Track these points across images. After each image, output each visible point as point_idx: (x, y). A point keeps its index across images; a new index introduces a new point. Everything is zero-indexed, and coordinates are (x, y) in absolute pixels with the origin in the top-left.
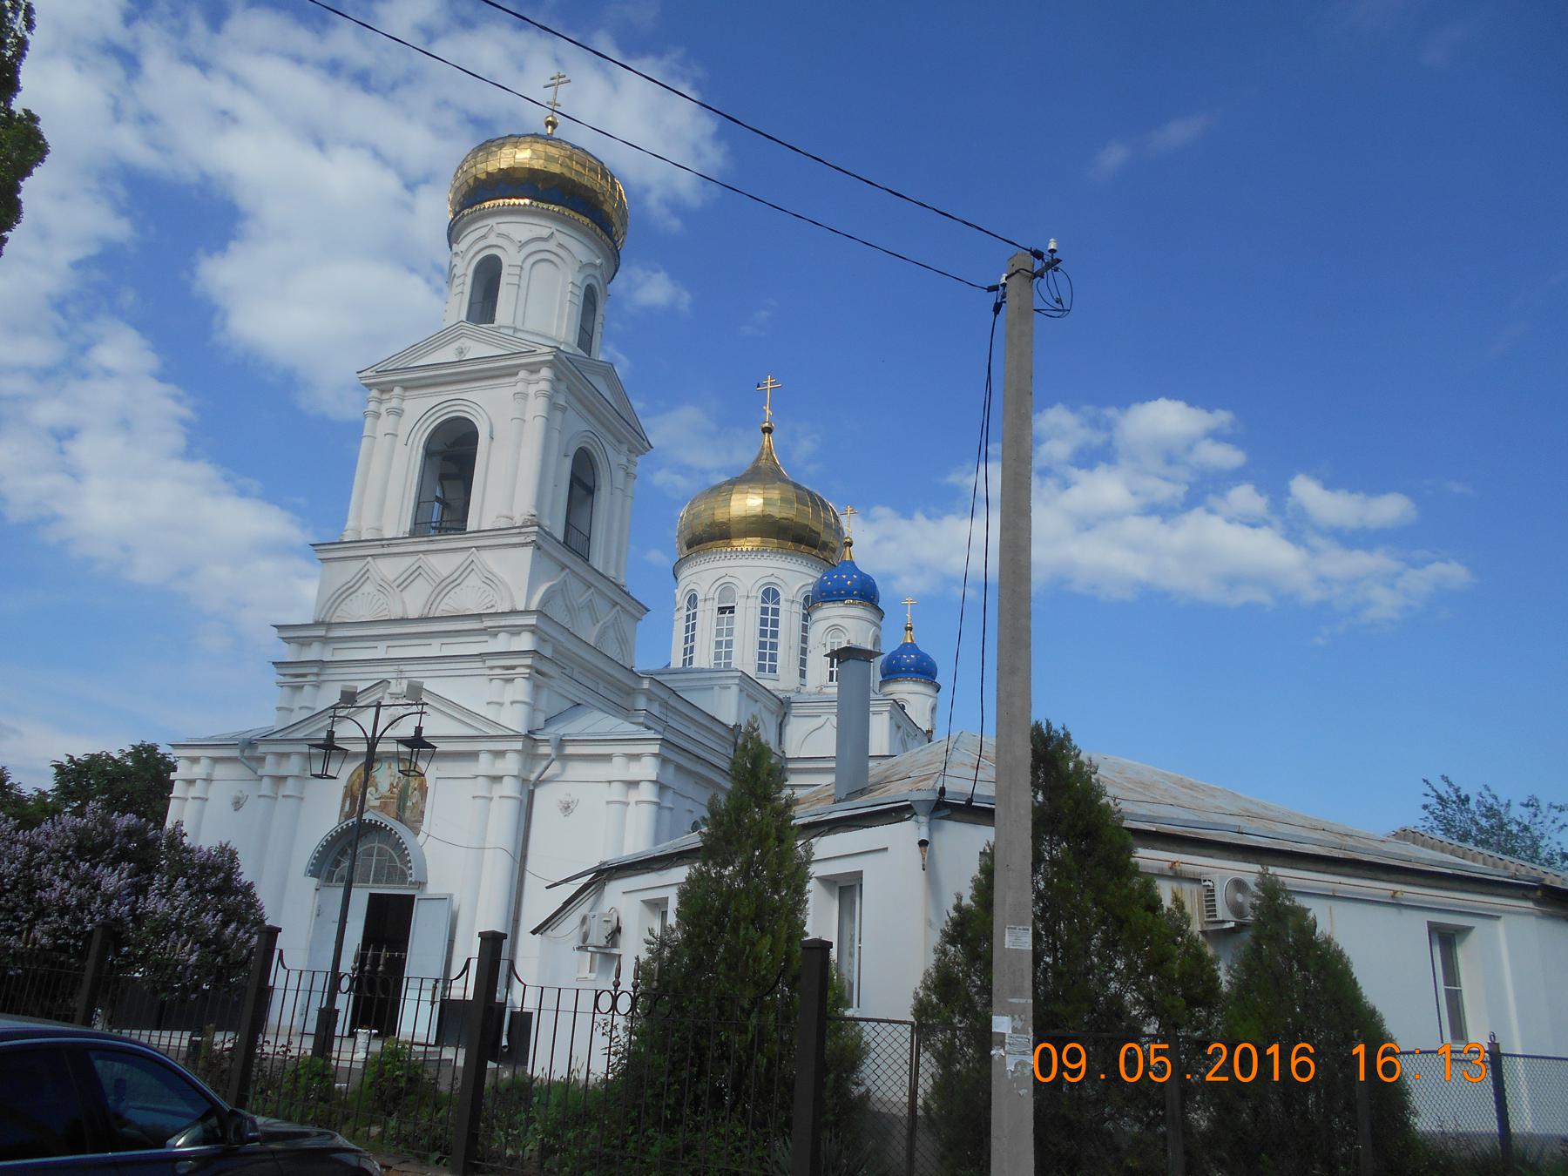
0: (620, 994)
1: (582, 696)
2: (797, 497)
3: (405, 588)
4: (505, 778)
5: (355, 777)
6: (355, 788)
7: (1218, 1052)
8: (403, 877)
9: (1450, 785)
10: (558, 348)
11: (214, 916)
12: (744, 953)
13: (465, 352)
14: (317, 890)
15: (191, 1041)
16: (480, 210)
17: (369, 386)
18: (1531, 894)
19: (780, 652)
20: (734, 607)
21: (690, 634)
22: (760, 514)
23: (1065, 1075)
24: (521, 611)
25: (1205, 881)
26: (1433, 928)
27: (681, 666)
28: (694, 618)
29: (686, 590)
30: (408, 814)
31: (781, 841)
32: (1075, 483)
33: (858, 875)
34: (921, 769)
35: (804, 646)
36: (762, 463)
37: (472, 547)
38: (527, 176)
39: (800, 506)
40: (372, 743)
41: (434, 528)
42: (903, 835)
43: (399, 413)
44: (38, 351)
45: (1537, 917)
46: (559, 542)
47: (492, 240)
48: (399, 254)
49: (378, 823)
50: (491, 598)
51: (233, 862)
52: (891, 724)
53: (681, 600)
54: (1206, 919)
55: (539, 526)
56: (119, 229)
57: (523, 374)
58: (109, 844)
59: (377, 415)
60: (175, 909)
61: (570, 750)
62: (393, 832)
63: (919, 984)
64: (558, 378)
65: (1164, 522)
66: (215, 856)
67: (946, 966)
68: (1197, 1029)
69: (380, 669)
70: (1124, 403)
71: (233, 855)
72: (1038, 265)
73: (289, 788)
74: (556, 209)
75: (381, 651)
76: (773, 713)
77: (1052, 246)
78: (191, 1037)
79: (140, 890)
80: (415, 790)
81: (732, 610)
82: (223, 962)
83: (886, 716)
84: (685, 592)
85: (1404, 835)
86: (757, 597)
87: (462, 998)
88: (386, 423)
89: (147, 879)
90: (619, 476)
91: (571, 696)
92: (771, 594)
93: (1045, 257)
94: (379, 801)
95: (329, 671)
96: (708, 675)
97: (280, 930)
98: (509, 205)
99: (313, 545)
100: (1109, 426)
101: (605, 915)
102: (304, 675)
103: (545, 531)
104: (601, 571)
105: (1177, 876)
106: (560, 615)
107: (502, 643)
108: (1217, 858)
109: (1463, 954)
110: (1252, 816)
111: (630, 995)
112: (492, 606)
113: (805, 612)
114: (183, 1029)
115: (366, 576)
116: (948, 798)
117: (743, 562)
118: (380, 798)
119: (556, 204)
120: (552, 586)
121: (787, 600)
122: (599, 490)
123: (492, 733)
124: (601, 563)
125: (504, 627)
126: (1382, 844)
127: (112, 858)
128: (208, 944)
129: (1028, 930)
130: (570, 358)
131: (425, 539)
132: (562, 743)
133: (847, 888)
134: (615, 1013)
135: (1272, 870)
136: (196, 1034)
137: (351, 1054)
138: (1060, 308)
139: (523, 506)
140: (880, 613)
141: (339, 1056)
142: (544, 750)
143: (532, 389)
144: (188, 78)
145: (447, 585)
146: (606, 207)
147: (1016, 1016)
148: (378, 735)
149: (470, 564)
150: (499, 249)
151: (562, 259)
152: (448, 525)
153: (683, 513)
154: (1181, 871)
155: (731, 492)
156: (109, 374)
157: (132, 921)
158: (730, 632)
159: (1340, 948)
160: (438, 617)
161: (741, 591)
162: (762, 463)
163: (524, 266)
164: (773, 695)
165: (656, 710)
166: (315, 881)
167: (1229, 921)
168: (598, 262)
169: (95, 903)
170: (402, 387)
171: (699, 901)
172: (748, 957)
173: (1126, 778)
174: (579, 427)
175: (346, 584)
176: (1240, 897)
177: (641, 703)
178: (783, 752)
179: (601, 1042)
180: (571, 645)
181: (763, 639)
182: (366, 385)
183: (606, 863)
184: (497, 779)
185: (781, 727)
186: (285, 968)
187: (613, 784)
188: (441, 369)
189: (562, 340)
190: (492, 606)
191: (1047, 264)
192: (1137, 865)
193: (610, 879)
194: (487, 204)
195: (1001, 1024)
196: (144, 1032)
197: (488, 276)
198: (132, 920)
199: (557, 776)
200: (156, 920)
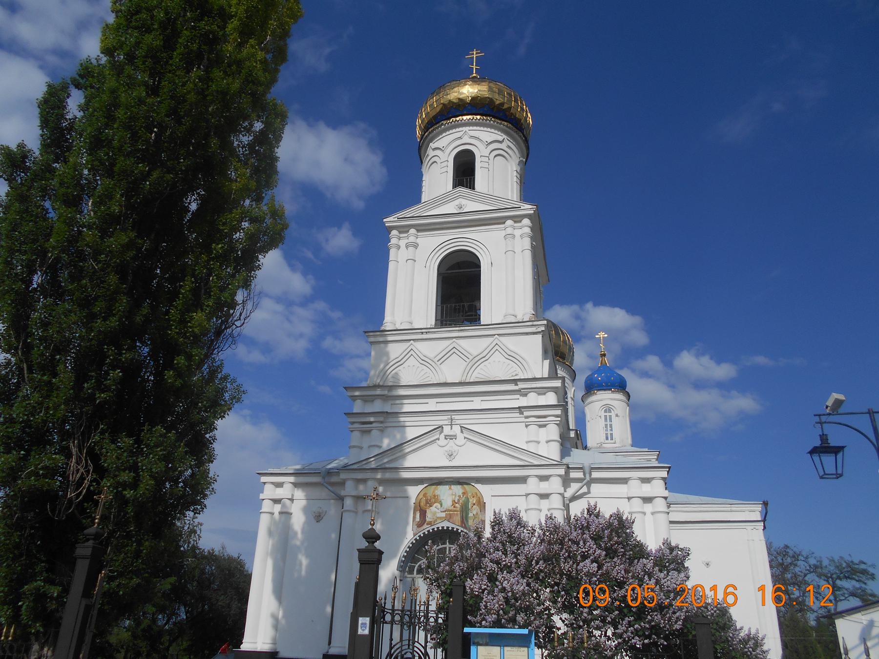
5: (421, 496)
6: (422, 504)
14: (401, 580)
24: (540, 378)
30: (470, 522)
37: (495, 335)
47: (466, 139)
70: (597, 304)
80: (474, 504)
87: (478, 647)
95: (391, 420)
107: (533, 399)
112: (516, 375)
123: (536, 463)
143: (518, 233)
151: (510, 156)
184: (544, 496)
190: (516, 375)
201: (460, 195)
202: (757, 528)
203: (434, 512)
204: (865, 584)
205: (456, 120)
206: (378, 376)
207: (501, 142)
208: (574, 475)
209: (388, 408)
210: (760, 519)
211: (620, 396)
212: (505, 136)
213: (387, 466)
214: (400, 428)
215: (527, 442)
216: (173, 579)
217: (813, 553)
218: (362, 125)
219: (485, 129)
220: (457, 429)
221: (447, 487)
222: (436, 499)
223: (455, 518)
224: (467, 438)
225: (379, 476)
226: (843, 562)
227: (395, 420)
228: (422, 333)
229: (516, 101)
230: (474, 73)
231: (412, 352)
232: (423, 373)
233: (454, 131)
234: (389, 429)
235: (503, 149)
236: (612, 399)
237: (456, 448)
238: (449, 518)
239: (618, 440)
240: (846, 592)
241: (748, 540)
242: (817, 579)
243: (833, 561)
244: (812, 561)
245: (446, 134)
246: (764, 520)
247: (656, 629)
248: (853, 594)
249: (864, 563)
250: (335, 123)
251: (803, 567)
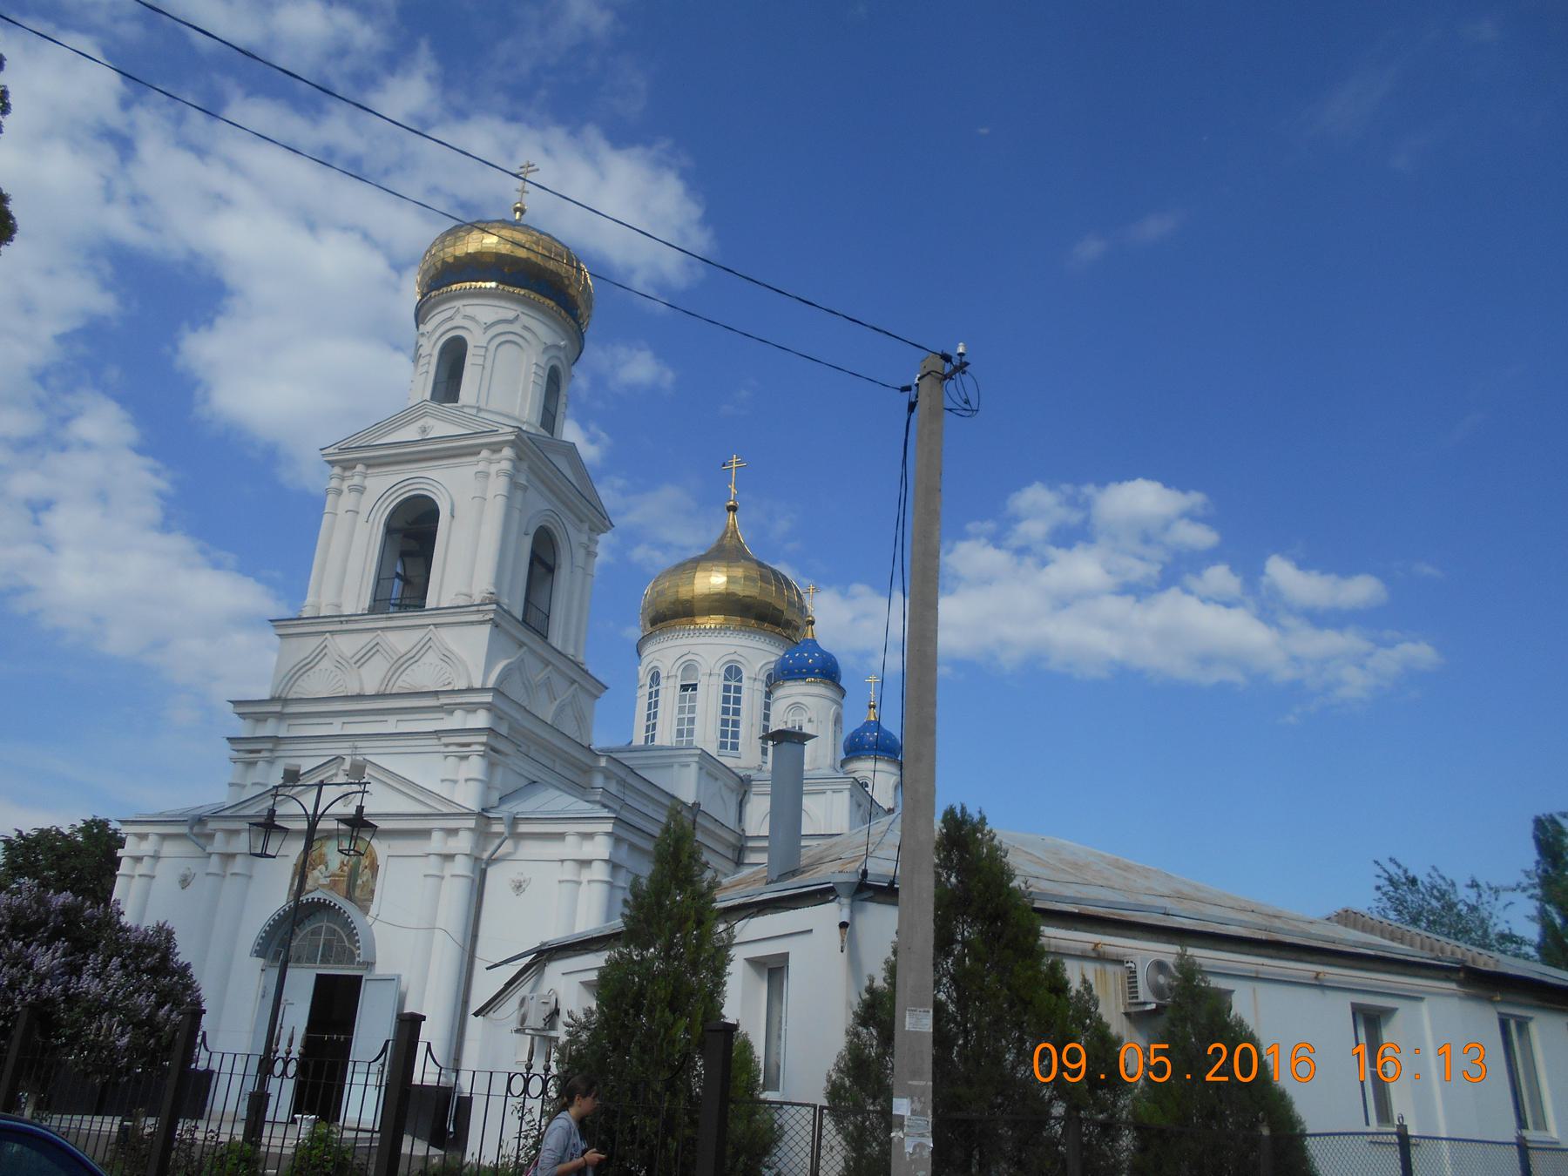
0: (532, 1077)
1: (539, 774)
2: (760, 575)
3: (362, 664)
4: (457, 856)
7: (1218, 1051)
8: (350, 957)
9: (1399, 866)
10: (520, 428)
11: (148, 997)
12: (659, 1036)
14: (262, 970)
15: (121, 1125)
16: (447, 292)
17: (332, 463)
18: (1454, 976)
19: (742, 730)
20: (696, 685)
21: (652, 711)
22: (724, 592)
23: (1065, 1074)
25: (1127, 962)
26: (1358, 1011)
27: (643, 743)
28: (657, 696)
29: (650, 667)
30: (358, 893)
31: (700, 923)
32: (1053, 561)
33: (785, 957)
34: (853, 851)
35: (766, 723)
36: (727, 541)
37: (430, 625)
38: (493, 260)
39: (764, 585)
40: (313, 820)
41: (394, 605)
42: (828, 915)
43: (360, 490)
44: (15, 422)
45: (1460, 998)
46: (517, 620)
47: (458, 321)
48: (379, 331)
49: (327, 902)
50: (447, 675)
51: (169, 942)
52: (851, 802)
53: (645, 679)
54: (1129, 1001)
55: (498, 604)
56: (103, 303)
57: (485, 453)
58: (45, 923)
59: (339, 492)
60: (108, 989)
61: (523, 828)
62: (342, 911)
63: (833, 1067)
64: (519, 458)
65: (1138, 600)
66: (152, 936)
67: (857, 1047)
68: (1101, 1112)
70: (1102, 484)
71: (170, 934)
72: (948, 368)
73: (239, 865)
74: (522, 292)
75: (336, 728)
76: (733, 791)
77: (961, 350)
78: (122, 1122)
79: (75, 970)
80: (366, 868)
81: (694, 687)
82: (156, 1044)
83: (846, 794)
84: (648, 670)
85: (1347, 918)
86: (719, 675)
88: (348, 500)
89: (83, 959)
90: (580, 554)
91: (525, 774)
92: (733, 672)
93: (953, 360)
94: (328, 879)
95: (283, 747)
96: (669, 753)
97: (424, 1018)
98: (475, 288)
99: (271, 621)
100: (1086, 505)
101: (545, 996)
102: (259, 751)
103: (503, 609)
104: (559, 649)
105: (1099, 957)
106: (516, 692)
107: (457, 720)
108: (1140, 940)
109: (1387, 1034)
110: (1180, 897)
111: (541, 1077)
112: (449, 683)
113: (767, 689)
114: (114, 1115)
115: (324, 652)
116: (870, 880)
117: (707, 640)
118: (330, 877)
119: (522, 287)
120: (508, 664)
121: (749, 678)
122: (559, 567)
123: (445, 810)
124: (560, 642)
126: (1310, 926)
127: (47, 937)
128: (133, 1021)
129: (928, 1012)
130: (532, 438)
131: (384, 616)
132: (515, 821)
133: (773, 970)
134: (527, 1096)
135: (1190, 951)
136: (127, 1118)
137: (110, 1126)
138: (968, 408)
139: (483, 584)
140: (842, 692)
141: (270, 1142)
142: (497, 828)
143: (494, 468)
144: (182, 165)
145: (402, 663)
146: (572, 291)
147: (916, 1098)
148: (320, 812)
149: (374, 646)
150: (464, 330)
151: (526, 340)
152: (407, 602)
153: (647, 590)
154: (1104, 953)
155: (695, 569)
156: (87, 446)
157: (64, 1001)
158: (692, 709)
159: (1250, 1030)
160: (395, 694)
161: (703, 669)
162: (727, 541)
163: (490, 347)
164: (733, 773)
165: (613, 788)
166: (261, 961)
167: (1150, 1003)
168: (562, 343)
169: (27, 983)
170: (365, 464)
171: (617, 984)
172: (663, 1040)
173: (1060, 859)
174: (540, 506)
175: (304, 660)
176: (1162, 979)
177: (599, 781)
178: (743, 830)
179: (513, 1124)
180: (528, 723)
181: (725, 717)
182: (329, 462)
183: (547, 943)
184: (449, 857)
185: (741, 805)
186: (207, 1050)
187: (566, 863)
188: (405, 447)
189: (525, 420)
190: (449, 683)
191: (956, 367)
192: (1042, 946)
193: (550, 959)
194: (454, 287)
195: (901, 1107)
196: (86, 1118)
197: (453, 357)
198: (64, 1000)
199: (509, 854)
200: (88, 1001)
201: (426, 412)
228: (341, 622)
236: (805, 695)
250: (621, 136)
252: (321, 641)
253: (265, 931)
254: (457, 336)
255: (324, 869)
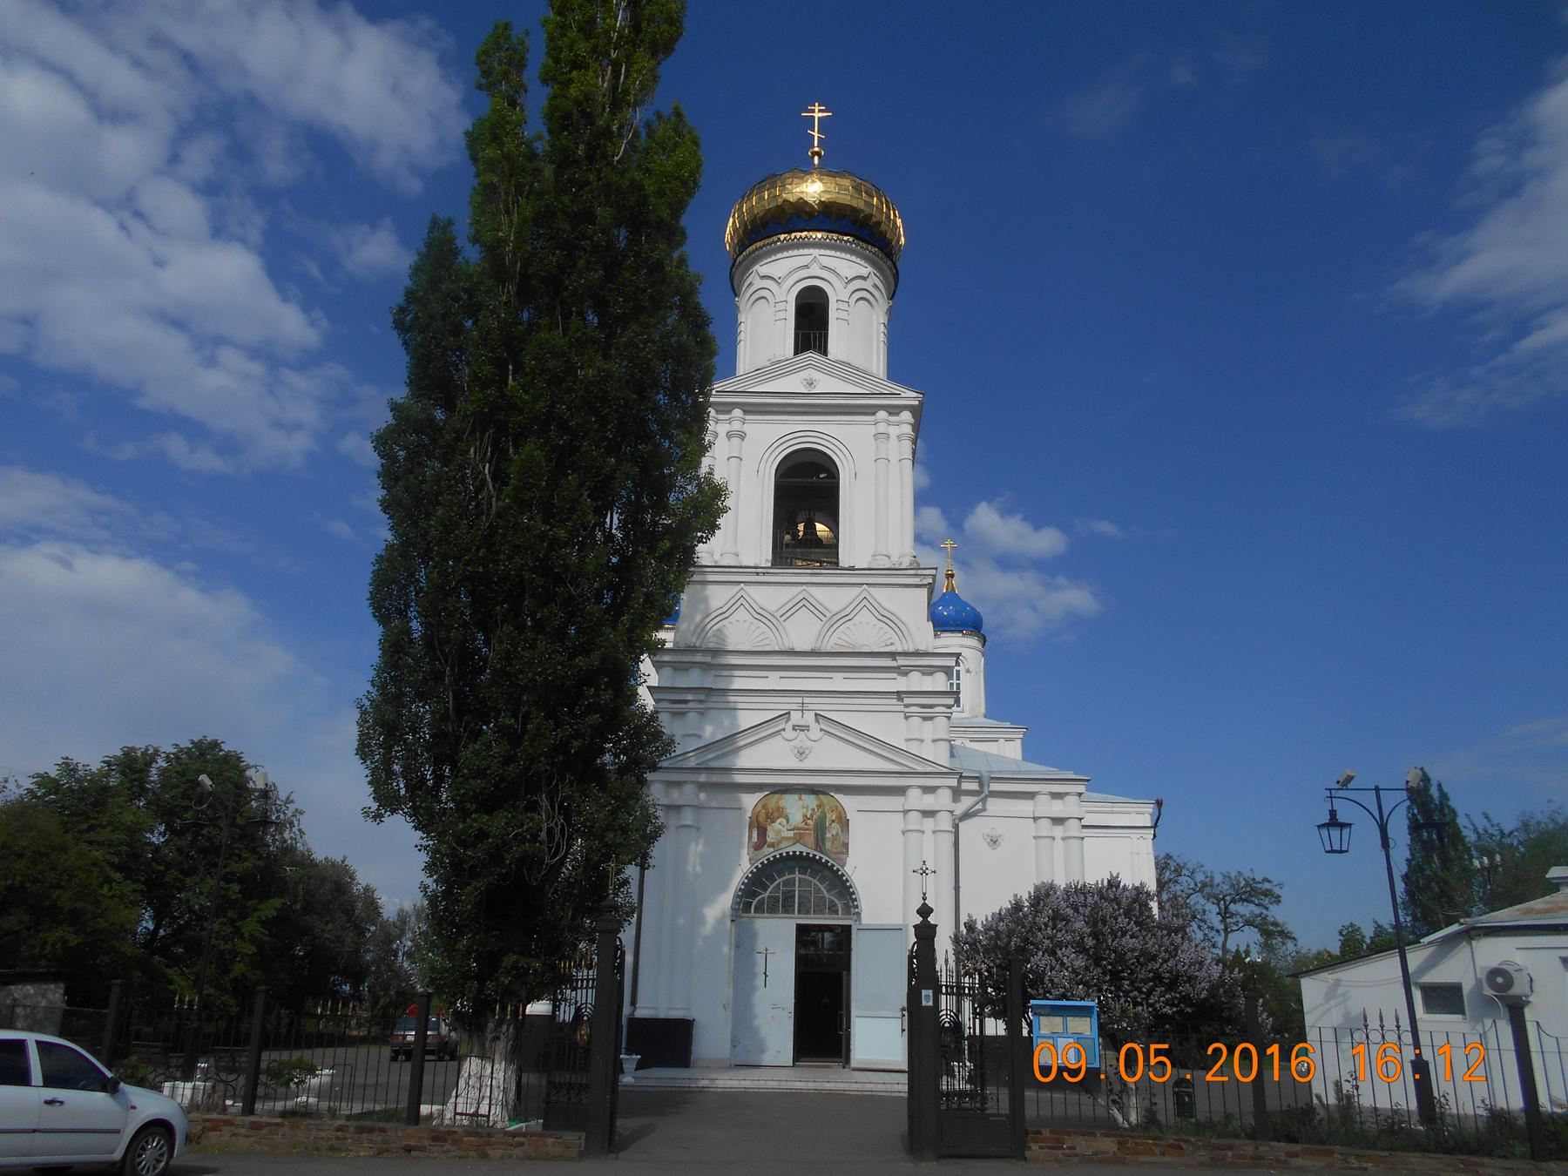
5: (759, 808)
6: (760, 819)
7: (1217, 1051)
13: (815, 384)
14: (732, 921)
30: (828, 845)
47: (815, 270)
69: (857, 701)
73: (688, 817)
94: (792, 833)
95: (714, 699)
107: (916, 682)
123: (920, 769)
125: (918, 666)
131: (809, 571)
143: (894, 431)
151: (876, 300)
190: (892, 644)
202: (1145, 836)
203: (777, 830)
204: (1267, 909)
205: (801, 237)
206: (694, 633)
207: (864, 278)
208: (966, 786)
209: (709, 681)
210: (1150, 825)
211: (973, 642)
212: (870, 269)
213: (712, 764)
214: (729, 711)
215: (907, 740)
216: (277, 902)
217: (1202, 866)
218: (426, 23)
219: (843, 255)
220: (809, 718)
221: (796, 796)
222: (780, 813)
223: (806, 839)
224: (825, 731)
225: (703, 778)
226: (1241, 879)
227: (723, 699)
229: (888, 207)
230: (816, 144)
231: (742, 600)
232: (758, 632)
233: (796, 252)
234: (713, 712)
235: (868, 289)
236: (962, 646)
237: (809, 744)
238: (798, 839)
239: (967, 708)
240: (1240, 920)
241: (1132, 853)
242: (1203, 901)
243: (1229, 877)
244: (1200, 877)
245: (783, 256)
246: (1155, 826)
247: (1185, 999)
248: (1248, 923)
249: (1269, 882)
251: (1185, 884)
252: (737, 591)
253: (743, 883)
254: (820, 287)
255: (784, 821)
